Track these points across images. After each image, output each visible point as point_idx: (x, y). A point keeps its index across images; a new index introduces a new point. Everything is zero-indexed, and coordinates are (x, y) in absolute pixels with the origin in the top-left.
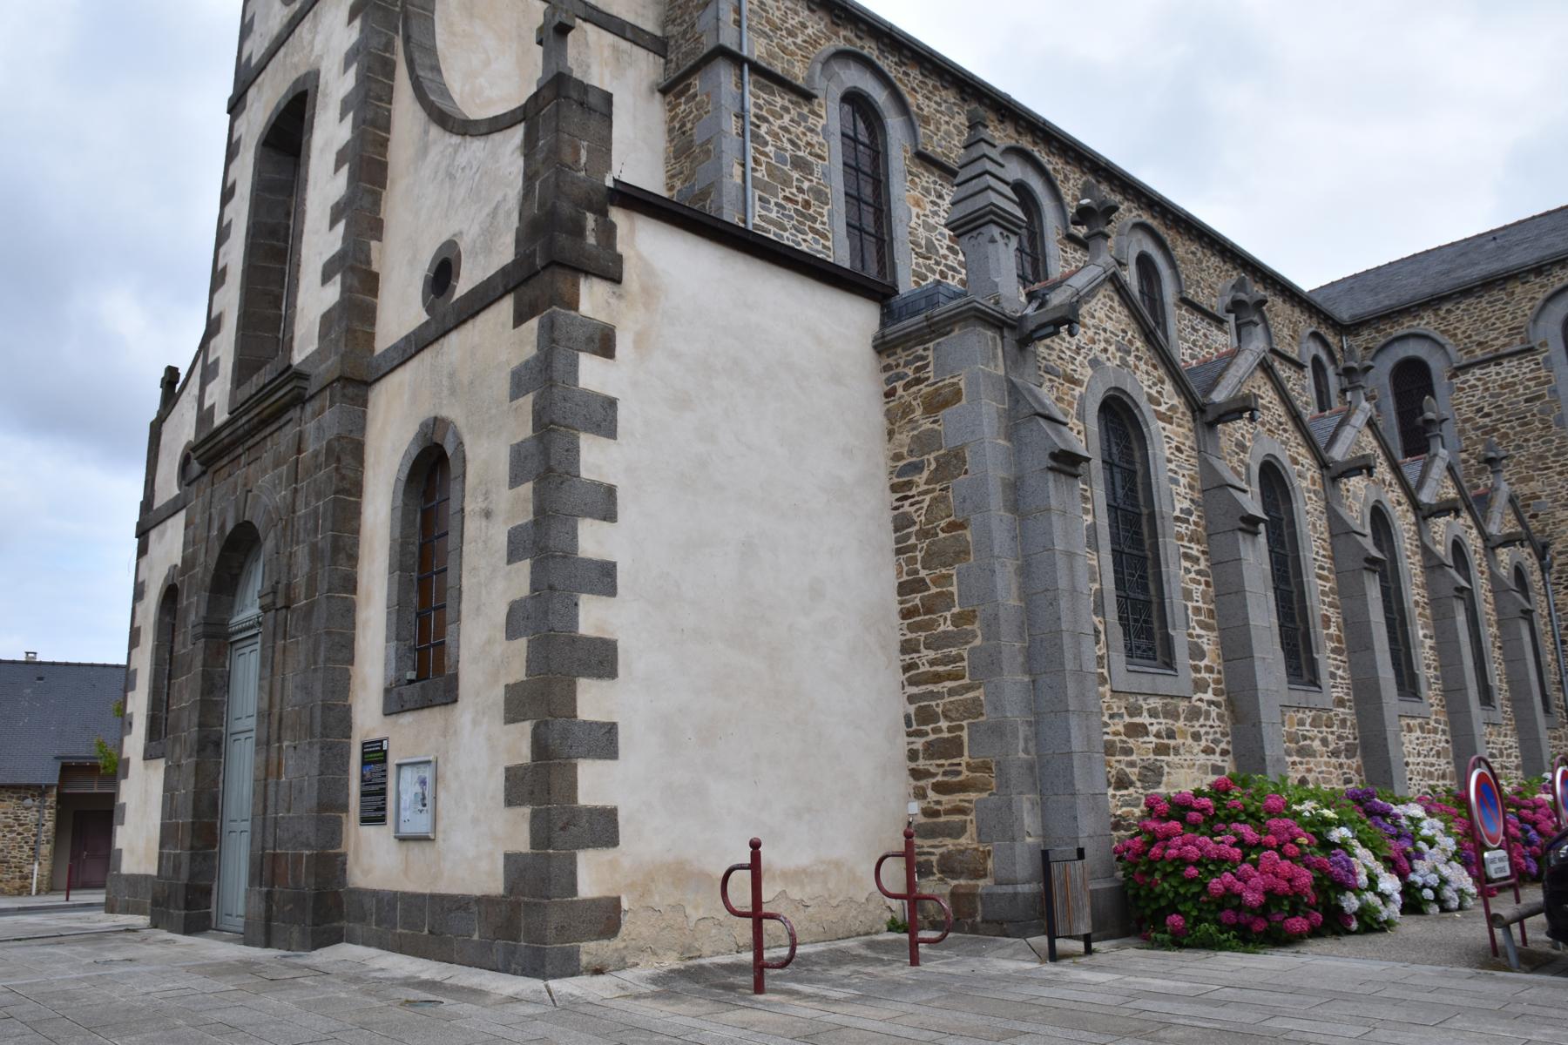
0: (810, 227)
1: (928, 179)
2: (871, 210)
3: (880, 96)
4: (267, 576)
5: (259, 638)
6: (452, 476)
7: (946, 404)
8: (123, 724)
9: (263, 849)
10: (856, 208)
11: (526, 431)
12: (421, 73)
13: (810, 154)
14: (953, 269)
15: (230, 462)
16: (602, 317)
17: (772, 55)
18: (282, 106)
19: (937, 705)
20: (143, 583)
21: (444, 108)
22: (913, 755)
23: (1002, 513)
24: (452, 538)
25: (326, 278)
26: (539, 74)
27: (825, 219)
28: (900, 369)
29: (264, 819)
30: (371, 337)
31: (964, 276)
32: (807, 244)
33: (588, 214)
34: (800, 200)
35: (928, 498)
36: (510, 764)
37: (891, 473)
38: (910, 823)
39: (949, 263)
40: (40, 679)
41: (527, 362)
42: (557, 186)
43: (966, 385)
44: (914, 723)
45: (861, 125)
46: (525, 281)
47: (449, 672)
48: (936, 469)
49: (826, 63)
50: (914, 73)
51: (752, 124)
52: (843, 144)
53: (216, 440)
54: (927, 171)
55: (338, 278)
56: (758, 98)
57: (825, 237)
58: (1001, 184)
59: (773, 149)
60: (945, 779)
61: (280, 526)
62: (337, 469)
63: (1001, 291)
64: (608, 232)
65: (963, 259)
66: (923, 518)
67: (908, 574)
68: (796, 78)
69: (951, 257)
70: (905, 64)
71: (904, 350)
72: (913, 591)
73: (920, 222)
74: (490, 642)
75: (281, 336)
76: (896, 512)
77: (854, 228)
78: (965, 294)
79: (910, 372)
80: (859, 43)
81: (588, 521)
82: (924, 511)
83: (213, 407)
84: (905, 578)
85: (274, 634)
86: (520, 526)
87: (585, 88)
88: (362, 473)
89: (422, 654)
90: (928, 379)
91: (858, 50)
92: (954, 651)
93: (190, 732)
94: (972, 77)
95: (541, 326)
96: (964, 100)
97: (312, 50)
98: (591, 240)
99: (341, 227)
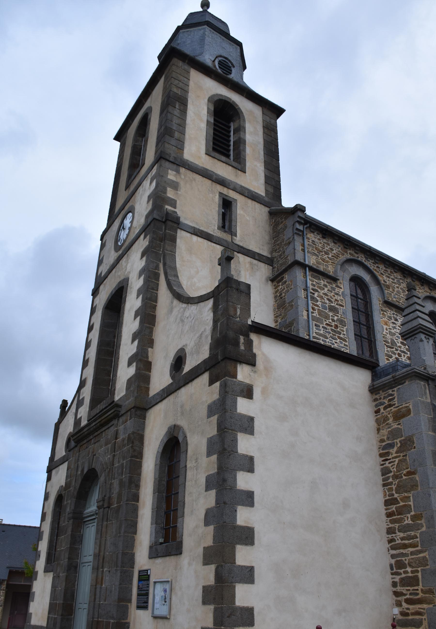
0: (338, 337)
1: (390, 312)
2: (365, 327)
3: (367, 277)
4: (100, 493)
5: (96, 520)
6: (182, 451)
7: (403, 416)
8: (36, 555)
9: (93, 618)
10: (358, 327)
11: (214, 432)
12: (170, 278)
13: (337, 304)
14: (404, 352)
15: (87, 442)
16: (247, 381)
17: (318, 263)
18: (113, 293)
19: (406, 560)
20: (48, 493)
21: (179, 292)
22: (394, 584)
23: (432, 467)
24: (181, 479)
25: (130, 364)
26: (219, 277)
27: (345, 333)
28: (382, 400)
29: (94, 604)
30: (148, 389)
31: (409, 355)
32: (337, 344)
33: (241, 336)
34: (333, 325)
35: (397, 460)
36: (204, 584)
37: (379, 448)
38: (394, 619)
39: (402, 349)
40: (3, 531)
41: (215, 401)
42: (228, 325)
43: (412, 407)
44: (394, 568)
45: (359, 291)
46: (214, 366)
47: (178, 540)
48: (400, 447)
49: (342, 265)
50: (382, 266)
51: (311, 293)
52: (351, 299)
53: (82, 432)
54: (390, 309)
55: (134, 364)
56: (313, 282)
57: (345, 341)
58: (424, 315)
59: (320, 303)
60: (411, 597)
61: (107, 471)
62: (132, 447)
63: (427, 363)
64: (249, 344)
65: (408, 347)
66: (395, 469)
67: (389, 496)
68: (330, 272)
69: (403, 347)
70: (377, 263)
71: (383, 392)
72: (391, 504)
73: (388, 332)
74: (197, 527)
75: (110, 388)
76: (382, 467)
77: (358, 336)
78: (409, 365)
79: (386, 401)
80: (356, 255)
81: (241, 472)
82: (395, 466)
83: (81, 418)
84: (388, 498)
85: (103, 519)
86: (211, 474)
87: (239, 283)
88: (143, 448)
89: (167, 531)
90: (394, 404)
91: (356, 258)
92: (413, 533)
93: (64, 561)
94: (407, 267)
95: (221, 386)
96: (404, 277)
97: (126, 270)
98: (242, 348)
99: (136, 343)
